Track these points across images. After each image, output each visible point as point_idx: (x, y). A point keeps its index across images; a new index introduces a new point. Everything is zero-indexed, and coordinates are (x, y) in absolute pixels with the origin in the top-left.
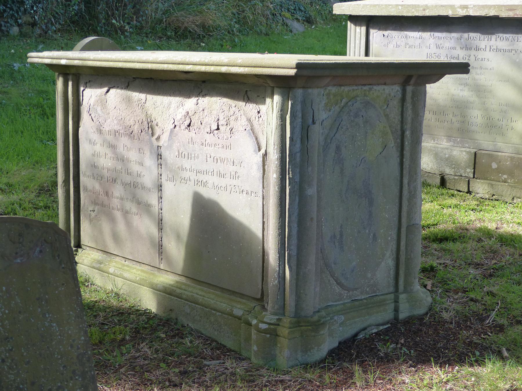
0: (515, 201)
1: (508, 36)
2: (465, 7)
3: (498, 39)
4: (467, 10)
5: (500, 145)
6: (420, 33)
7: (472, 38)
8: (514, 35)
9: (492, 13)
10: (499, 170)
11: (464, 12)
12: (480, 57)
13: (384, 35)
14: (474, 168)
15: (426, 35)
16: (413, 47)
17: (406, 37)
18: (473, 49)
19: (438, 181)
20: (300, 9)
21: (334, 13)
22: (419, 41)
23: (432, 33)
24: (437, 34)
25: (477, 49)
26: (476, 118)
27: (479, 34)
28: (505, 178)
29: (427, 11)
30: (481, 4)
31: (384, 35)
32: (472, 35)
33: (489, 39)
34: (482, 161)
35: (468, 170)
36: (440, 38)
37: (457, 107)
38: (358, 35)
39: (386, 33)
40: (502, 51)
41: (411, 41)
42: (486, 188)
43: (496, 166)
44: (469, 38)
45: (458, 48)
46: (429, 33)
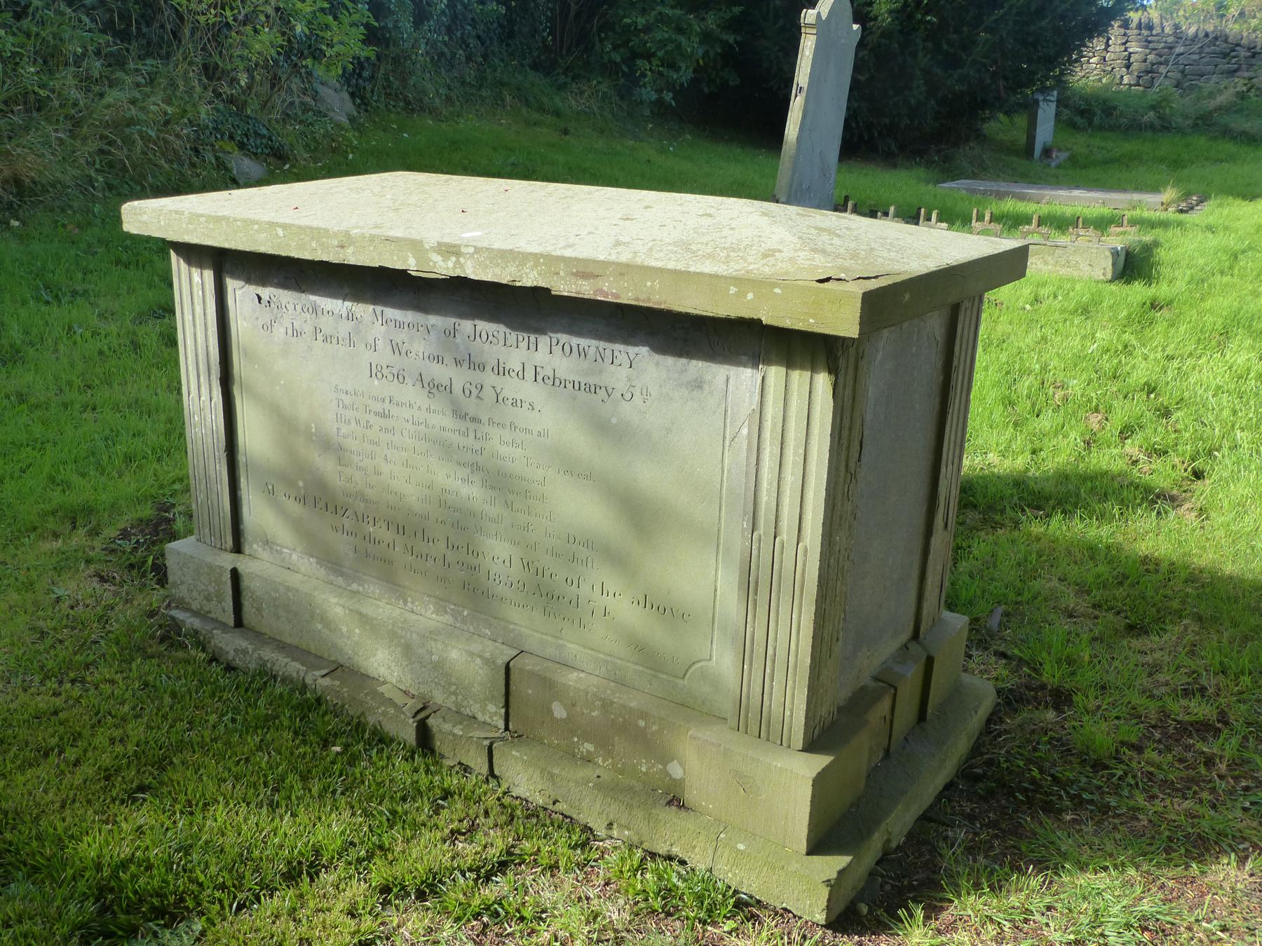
0: (615, 833)
1: (584, 342)
2: (451, 250)
3: (557, 350)
4: (458, 262)
5: (572, 649)
6: (348, 304)
7: (484, 336)
8: (602, 344)
9: (529, 278)
10: (570, 727)
11: (450, 264)
12: (507, 393)
13: (260, 299)
14: (507, 705)
15: (364, 311)
16: (334, 341)
17: (315, 310)
18: (488, 368)
19: (409, 734)
20: (257, 134)
21: (127, 227)
22: (345, 328)
23: (379, 308)
24: (392, 313)
25: (501, 371)
26: (507, 563)
27: (502, 328)
28: (588, 751)
29: (350, 250)
30: (496, 246)
31: (260, 299)
32: (483, 326)
33: (532, 347)
34: (525, 690)
35: (491, 708)
36: (399, 325)
37: (457, 525)
38: (198, 293)
39: (266, 292)
40: (570, 386)
41: (326, 324)
42: (536, 776)
43: (565, 715)
44: (476, 335)
45: (448, 359)
46: (371, 307)
